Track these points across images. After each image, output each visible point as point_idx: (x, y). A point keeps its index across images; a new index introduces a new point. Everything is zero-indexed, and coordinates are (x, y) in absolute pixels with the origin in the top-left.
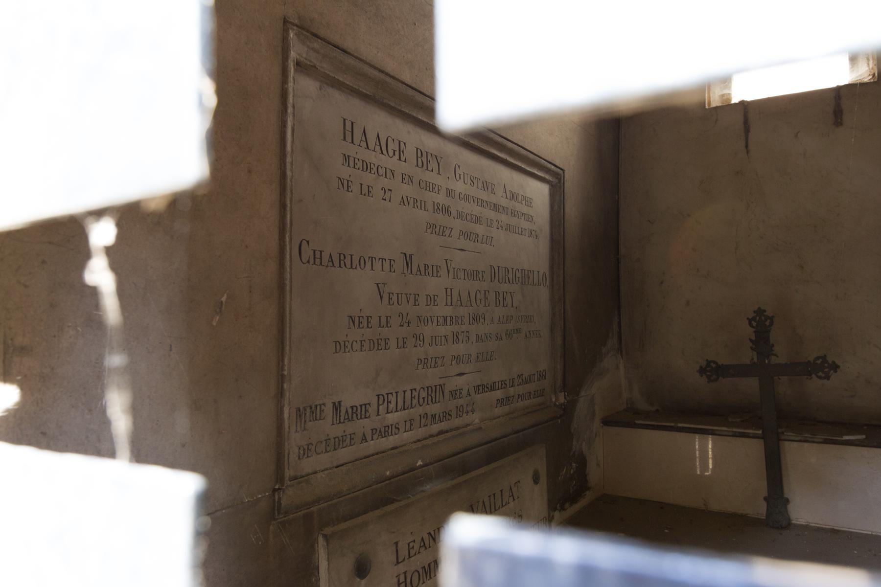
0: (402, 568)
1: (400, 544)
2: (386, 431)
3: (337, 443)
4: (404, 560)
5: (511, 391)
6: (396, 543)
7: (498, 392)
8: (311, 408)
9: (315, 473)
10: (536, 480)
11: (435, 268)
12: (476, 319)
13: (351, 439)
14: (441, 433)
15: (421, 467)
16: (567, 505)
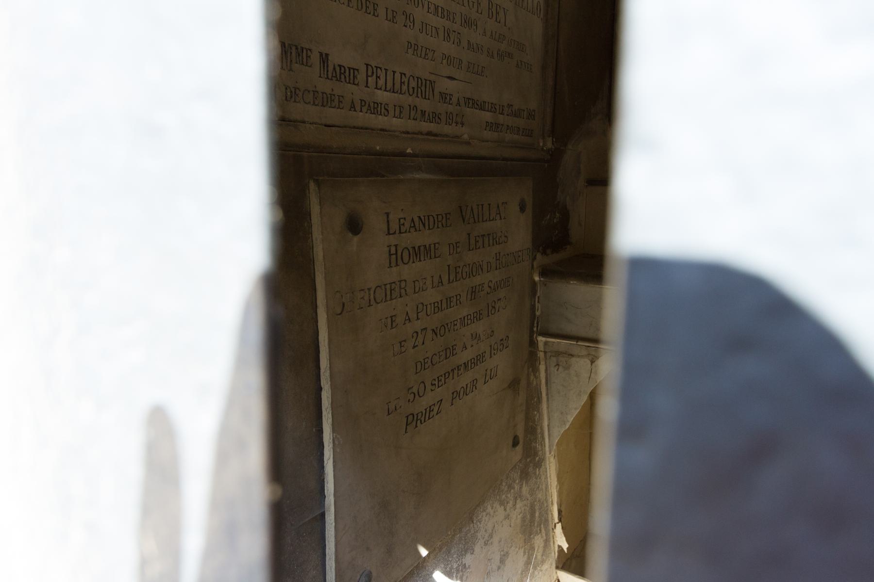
0: (393, 240)
1: (391, 216)
2: (375, 108)
3: (325, 100)
4: (395, 233)
5: (501, 119)
6: (388, 214)
7: (489, 114)
8: (297, 49)
9: (304, 122)
10: (522, 209)
11: (424, 49)
12: (468, 22)
13: (340, 102)
14: (429, 133)
15: (410, 155)
16: (549, 251)
